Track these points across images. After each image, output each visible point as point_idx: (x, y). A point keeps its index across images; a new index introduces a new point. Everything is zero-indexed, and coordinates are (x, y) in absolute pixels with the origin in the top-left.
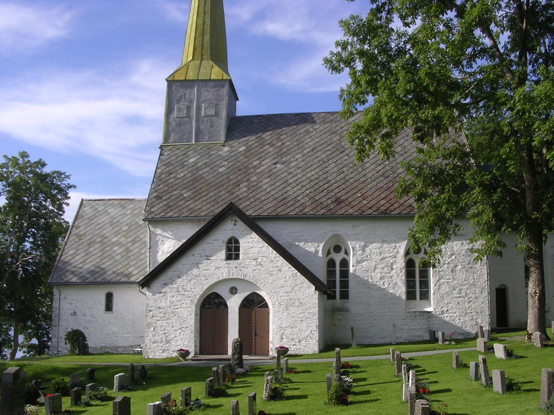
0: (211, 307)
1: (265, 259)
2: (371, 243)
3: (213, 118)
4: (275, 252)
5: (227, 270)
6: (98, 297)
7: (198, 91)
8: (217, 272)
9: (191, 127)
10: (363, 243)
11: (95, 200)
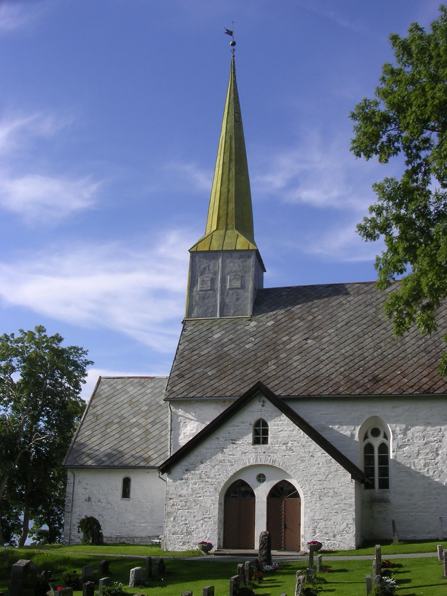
0: (237, 495)
1: (296, 444)
2: (413, 426)
3: (239, 291)
4: (306, 436)
5: (254, 455)
7: (222, 263)
8: (244, 457)
9: (216, 301)
10: (404, 426)
11: (114, 378)
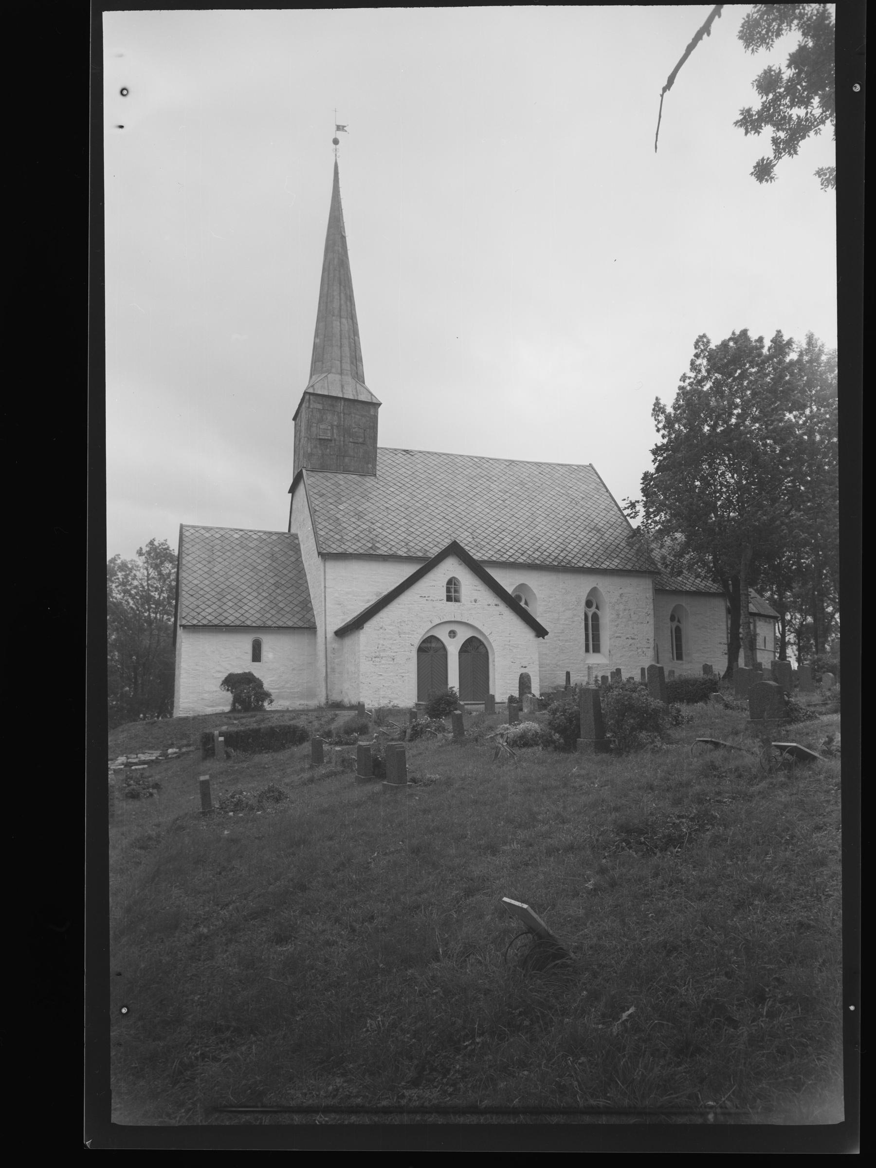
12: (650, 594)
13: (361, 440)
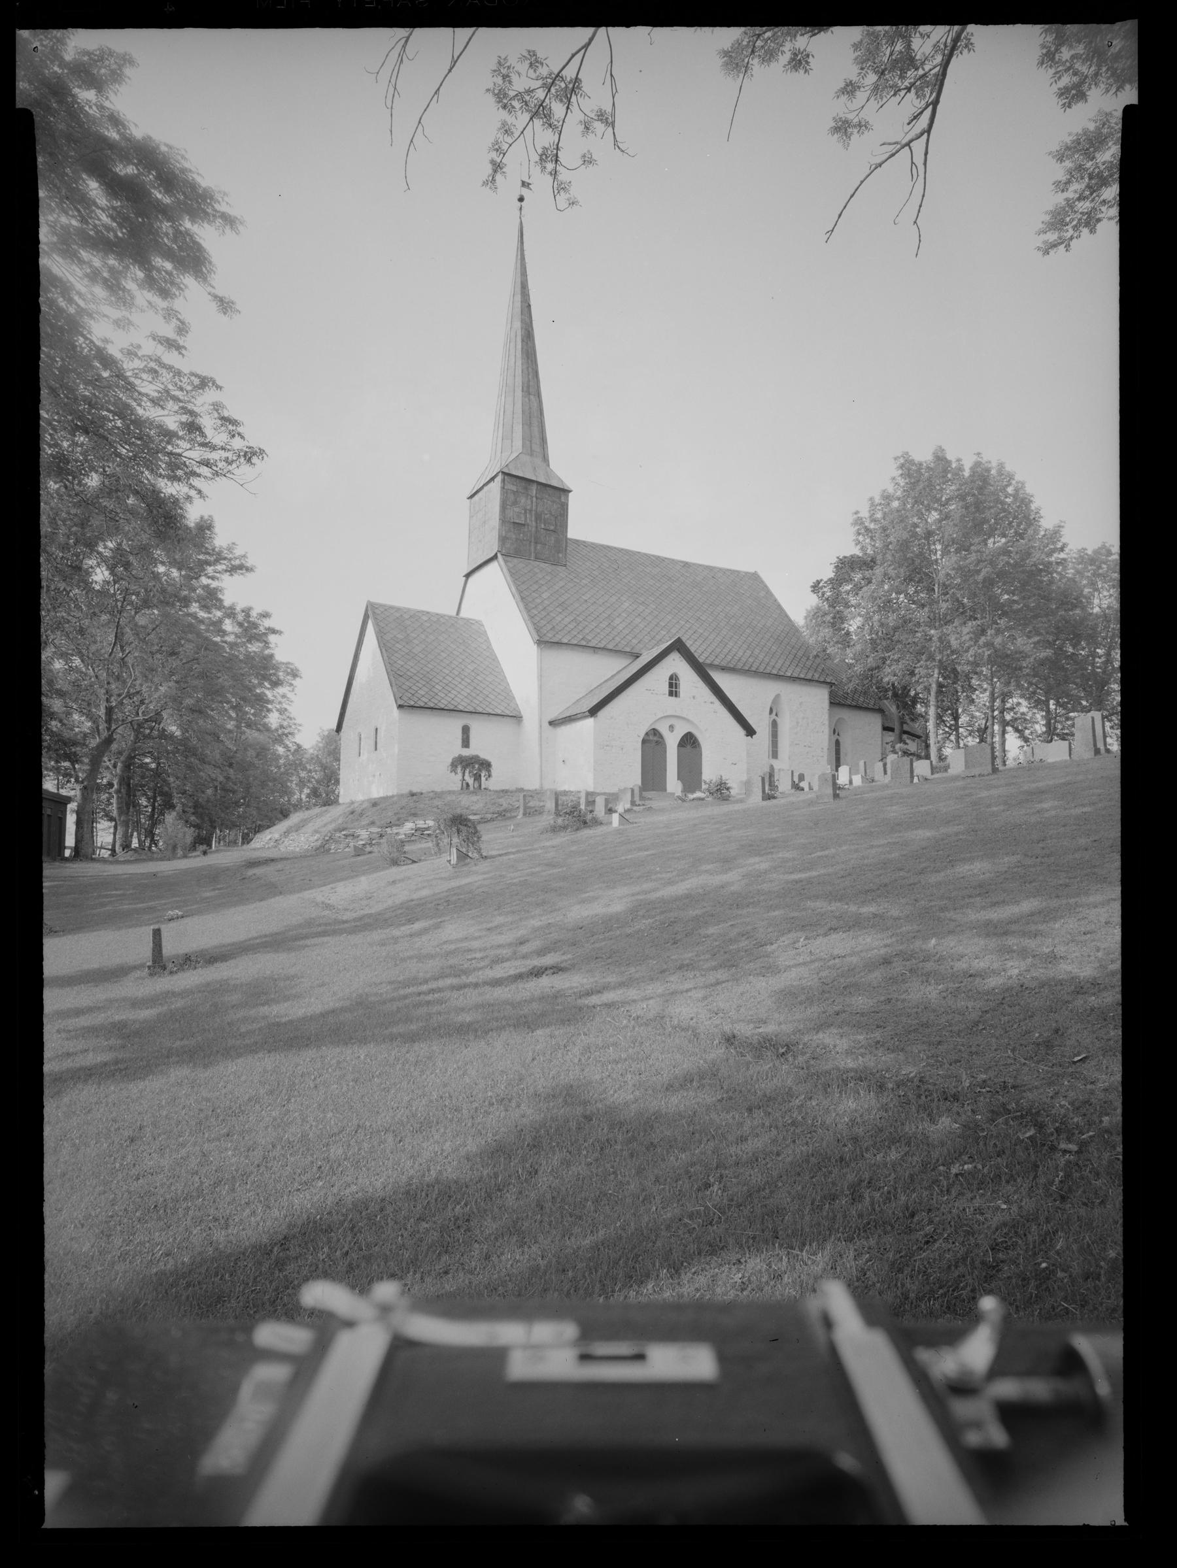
6: (451, 728)
12: (826, 703)
13: (552, 528)
